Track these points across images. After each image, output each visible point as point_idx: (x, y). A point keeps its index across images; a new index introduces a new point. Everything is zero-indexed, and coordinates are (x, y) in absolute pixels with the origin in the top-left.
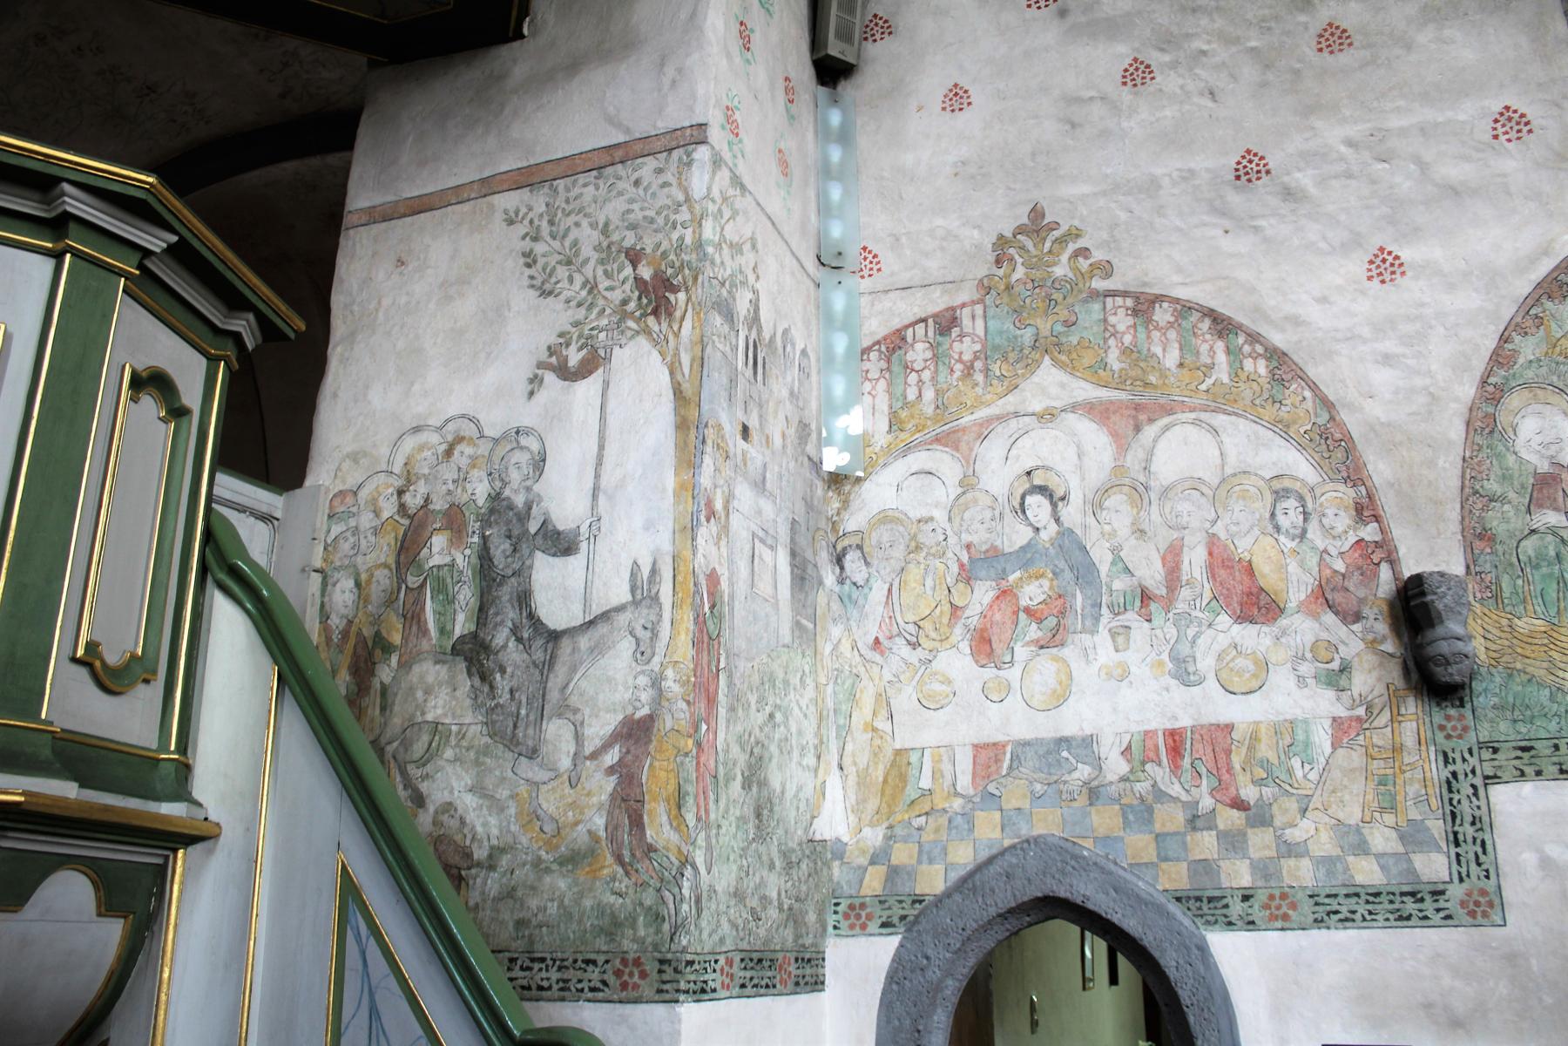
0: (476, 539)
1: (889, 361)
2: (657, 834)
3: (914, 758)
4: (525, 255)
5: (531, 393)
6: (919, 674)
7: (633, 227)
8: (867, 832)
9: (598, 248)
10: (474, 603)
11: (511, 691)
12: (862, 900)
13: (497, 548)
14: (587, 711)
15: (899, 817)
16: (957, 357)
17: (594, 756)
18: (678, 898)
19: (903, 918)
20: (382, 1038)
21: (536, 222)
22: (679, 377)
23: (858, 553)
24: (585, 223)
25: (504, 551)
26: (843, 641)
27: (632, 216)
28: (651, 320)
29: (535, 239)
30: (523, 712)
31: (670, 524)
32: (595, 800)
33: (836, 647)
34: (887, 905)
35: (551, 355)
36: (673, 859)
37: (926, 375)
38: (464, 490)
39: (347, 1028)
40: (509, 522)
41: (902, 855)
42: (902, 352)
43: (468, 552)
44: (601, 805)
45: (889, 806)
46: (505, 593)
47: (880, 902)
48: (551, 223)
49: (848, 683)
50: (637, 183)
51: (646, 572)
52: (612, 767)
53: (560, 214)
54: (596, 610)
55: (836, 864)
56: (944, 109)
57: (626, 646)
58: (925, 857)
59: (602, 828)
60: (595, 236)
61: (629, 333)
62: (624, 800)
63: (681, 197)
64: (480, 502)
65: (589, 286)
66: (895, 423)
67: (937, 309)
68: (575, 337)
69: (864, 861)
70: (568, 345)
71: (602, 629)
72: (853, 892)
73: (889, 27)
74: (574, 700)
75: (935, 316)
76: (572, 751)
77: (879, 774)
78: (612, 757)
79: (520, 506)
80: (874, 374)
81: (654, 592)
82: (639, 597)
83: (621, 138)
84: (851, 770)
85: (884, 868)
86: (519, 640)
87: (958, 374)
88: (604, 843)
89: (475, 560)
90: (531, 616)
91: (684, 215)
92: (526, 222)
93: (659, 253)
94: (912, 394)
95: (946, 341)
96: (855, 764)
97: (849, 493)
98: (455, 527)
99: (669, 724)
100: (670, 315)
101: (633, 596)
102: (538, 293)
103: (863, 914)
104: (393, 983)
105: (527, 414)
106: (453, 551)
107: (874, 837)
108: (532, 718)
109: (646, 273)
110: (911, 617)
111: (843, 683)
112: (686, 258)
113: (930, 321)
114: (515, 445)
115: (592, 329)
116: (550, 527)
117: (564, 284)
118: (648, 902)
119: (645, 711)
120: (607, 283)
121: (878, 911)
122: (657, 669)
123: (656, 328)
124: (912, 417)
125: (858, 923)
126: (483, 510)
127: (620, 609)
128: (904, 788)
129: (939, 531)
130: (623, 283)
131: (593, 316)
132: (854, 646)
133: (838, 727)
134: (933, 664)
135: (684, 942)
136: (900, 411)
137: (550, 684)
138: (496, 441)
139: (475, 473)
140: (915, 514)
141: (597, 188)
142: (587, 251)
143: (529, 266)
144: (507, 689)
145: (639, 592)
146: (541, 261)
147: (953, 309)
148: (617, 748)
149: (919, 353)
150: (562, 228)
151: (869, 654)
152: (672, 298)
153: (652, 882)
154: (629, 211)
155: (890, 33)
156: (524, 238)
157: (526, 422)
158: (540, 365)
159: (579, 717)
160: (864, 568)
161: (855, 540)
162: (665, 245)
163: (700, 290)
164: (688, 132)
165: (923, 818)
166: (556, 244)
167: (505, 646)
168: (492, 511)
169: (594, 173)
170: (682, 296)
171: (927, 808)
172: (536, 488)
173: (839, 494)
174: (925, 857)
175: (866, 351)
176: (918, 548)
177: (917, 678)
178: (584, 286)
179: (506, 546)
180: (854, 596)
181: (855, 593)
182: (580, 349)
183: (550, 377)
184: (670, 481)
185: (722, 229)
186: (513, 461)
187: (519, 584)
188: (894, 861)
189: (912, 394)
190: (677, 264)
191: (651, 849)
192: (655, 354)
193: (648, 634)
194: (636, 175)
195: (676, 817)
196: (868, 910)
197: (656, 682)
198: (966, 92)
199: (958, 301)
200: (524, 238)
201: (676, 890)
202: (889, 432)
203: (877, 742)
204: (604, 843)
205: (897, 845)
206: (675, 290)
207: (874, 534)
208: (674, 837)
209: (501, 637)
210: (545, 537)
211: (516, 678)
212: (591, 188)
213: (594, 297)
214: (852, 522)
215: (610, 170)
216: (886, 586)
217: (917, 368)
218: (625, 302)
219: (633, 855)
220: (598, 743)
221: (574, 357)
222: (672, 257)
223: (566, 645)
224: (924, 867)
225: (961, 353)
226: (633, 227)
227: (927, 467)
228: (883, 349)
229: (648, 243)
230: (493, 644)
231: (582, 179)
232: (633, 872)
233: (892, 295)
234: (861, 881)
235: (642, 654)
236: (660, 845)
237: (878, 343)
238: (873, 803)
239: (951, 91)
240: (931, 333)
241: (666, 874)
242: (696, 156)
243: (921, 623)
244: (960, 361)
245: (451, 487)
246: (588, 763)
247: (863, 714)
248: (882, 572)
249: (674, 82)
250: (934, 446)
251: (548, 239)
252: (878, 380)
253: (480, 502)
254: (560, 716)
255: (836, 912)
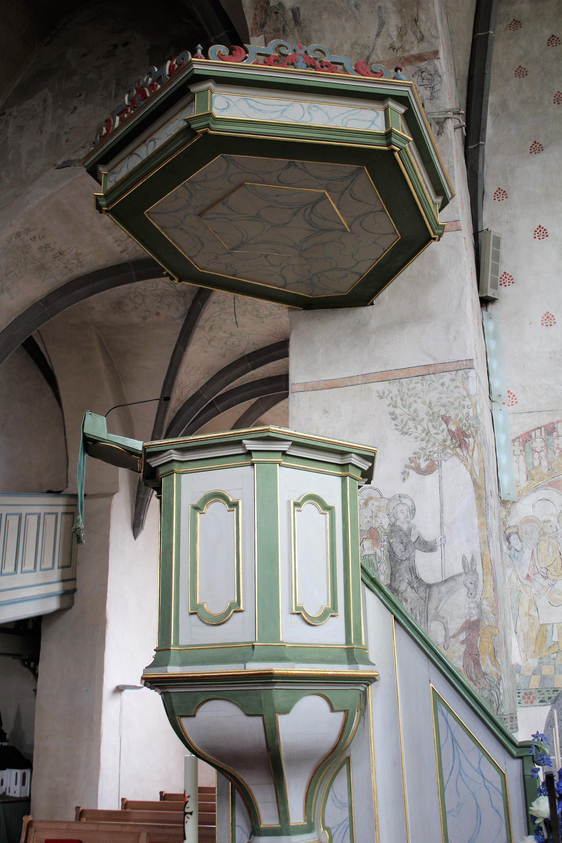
0: (385, 543)
1: (524, 446)
2: (486, 668)
3: (549, 628)
4: (390, 414)
5: (404, 479)
6: (549, 590)
7: (444, 406)
8: (530, 660)
9: (427, 414)
10: (388, 571)
11: (411, 610)
12: (530, 691)
13: (397, 548)
14: (448, 618)
15: (544, 654)
16: (556, 446)
17: (454, 636)
18: (498, 693)
19: (550, 698)
20: (458, 748)
21: (394, 398)
22: (475, 476)
23: (516, 536)
24: (419, 401)
25: (400, 549)
26: (513, 575)
27: (442, 400)
28: (458, 450)
29: (395, 407)
30: (418, 618)
31: (478, 540)
32: (457, 655)
33: (510, 578)
34: (542, 693)
35: (411, 462)
36: (495, 678)
37: (542, 454)
38: (376, 521)
39: (443, 746)
40: (401, 536)
41: (547, 670)
42: (530, 443)
43: (382, 549)
44: (459, 658)
45: (539, 649)
46: (403, 567)
47: (538, 691)
48: (402, 399)
49: (516, 594)
50: (442, 384)
51: (469, 560)
52: (463, 641)
53: (406, 396)
54: (448, 576)
55: (517, 675)
56: (542, 324)
57: (463, 591)
58: (557, 672)
59: (462, 666)
60: (425, 407)
61: (449, 455)
62: (470, 654)
63: (465, 394)
64: (386, 527)
65: (426, 432)
66: (529, 477)
67: (546, 423)
68: (422, 455)
69: (529, 673)
70: (419, 458)
71: (451, 583)
72: (526, 687)
73: (512, 279)
74: (442, 613)
75: (545, 426)
76: (444, 634)
77: (534, 634)
78: (463, 637)
79: (406, 529)
80: (518, 453)
81: (474, 568)
82: (467, 570)
83: (432, 362)
84: (520, 633)
85: (539, 676)
86: (413, 588)
87: (557, 454)
88: (463, 672)
89: (386, 553)
90: (417, 577)
91: (467, 402)
92: (389, 398)
93: (458, 419)
94: (536, 463)
95: (550, 438)
96: (522, 630)
97: (510, 508)
98: (374, 537)
99: (487, 623)
100: (467, 448)
101: (464, 570)
102: (401, 433)
103: (531, 697)
104: (460, 729)
105: (404, 489)
106: (375, 548)
107: (533, 663)
108: (423, 621)
109: (453, 428)
110: (543, 566)
111: (514, 595)
112: (471, 422)
113: (543, 429)
114: (399, 502)
115: (430, 452)
116: (422, 540)
117: (413, 429)
118: (486, 695)
119: (475, 618)
120: (435, 431)
121: (538, 695)
122: (479, 600)
123: (461, 454)
124: (537, 473)
125: (529, 701)
126: (387, 531)
127: (459, 575)
128: (545, 641)
129: (554, 526)
130: (442, 431)
131: (430, 446)
132: (518, 578)
133: (513, 614)
134: (555, 586)
135: (503, 711)
136: (531, 471)
137: (429, 607)
138: (390, 500)
139: (380, 514)
140: (542, 518)
141: (423, 385)
142: (422, 415)
143: (394, 419)
144: (409, 609)
145: (467, 568)
146: (400, 418)
147: (553, 423)
148: (464, 633)
149: (538, 443)
150: (408, 403)
151: (525, 582)
152: (467, 440)
153: (486, 687)
154: (440, 398)
155: (513, 283)
156: (389, 406)
157: (403, 492)
158: (406, 466)
159: (445, 620)
160: (520, 542)
161: (514, 530)
162: (460, 416)
163: (479, 438)
164: (465, 363)
165: (556, 654)
166: (406, 410)
167: (406, 590)
168: (392, 531)
169: (420, 377)
170: (471, 439)
171: (557, 650)
172: (412, 521)
173: (505, 509)
174: (557, 672)
175: (514, 441)
176: (544, 534)
177: (548, 592)
178: (423, 431)
179: (401, 547)
180: (516, 556)
181: (517, 554)
182: (426, 460)
183: (412, 473)
184: (476, 522)
185: (272, 265)
186: (399, 509)
187: (410, 564)
188: (543, 673)
189: (536, 463)
190: (467, 425)
191: (484, 674)
192: (462, 465)
193: (473, 586)
194: (442, 381)
195: (494, 661)
196: (533, 695)
197: (479, 606)
198: (553, 316)
199: (555, 420)
200: (389, 406)
201: (497, 690)
202: (527, 480)
203: (532, 621)
204: (463, 672)
205: (544, 666)
206: (468, 437)
207: (523, 527)
208: (494, 669)
209: (403, 586)
210: (420, 544)
211: (413, 604)
212: (419, 385)
213: (429, 437)
214: (512, 522)
215: (428, 377)
216: (531, 551)
217: (538, 451)
218: (445, 441)
219: (477, 677)
220: (455, 631)
221: (423, 465)
222: (464, 421)
223: (435, 590)
224: (557, 676)
225: (558, 445)
226: (444, 406)
227: (546, 498)
228: (521, 440)
229: (452, 414)
230: (400, 589)
231: (414, 380)
232: (477, 684)
233: (523, 415)
234: (529, 682)
235: (471, 594)
236: (488, 672)
237: (518, 438)
238: (532, 648)
239: (545, 315)
240: (543, 434)
241: (492, 684)
242: (470, 374)
243: (548, 568)
244: (558, 448)
245: (369, 519)
246: (452, 639)
247: (524, 609)
248: (528, 545)
249: (455, 338)
250: (549, 488)
251: (402, 407)
252: (519, 455)
253: (386, 527)
254: (436, 620)
255: (519, 696)
